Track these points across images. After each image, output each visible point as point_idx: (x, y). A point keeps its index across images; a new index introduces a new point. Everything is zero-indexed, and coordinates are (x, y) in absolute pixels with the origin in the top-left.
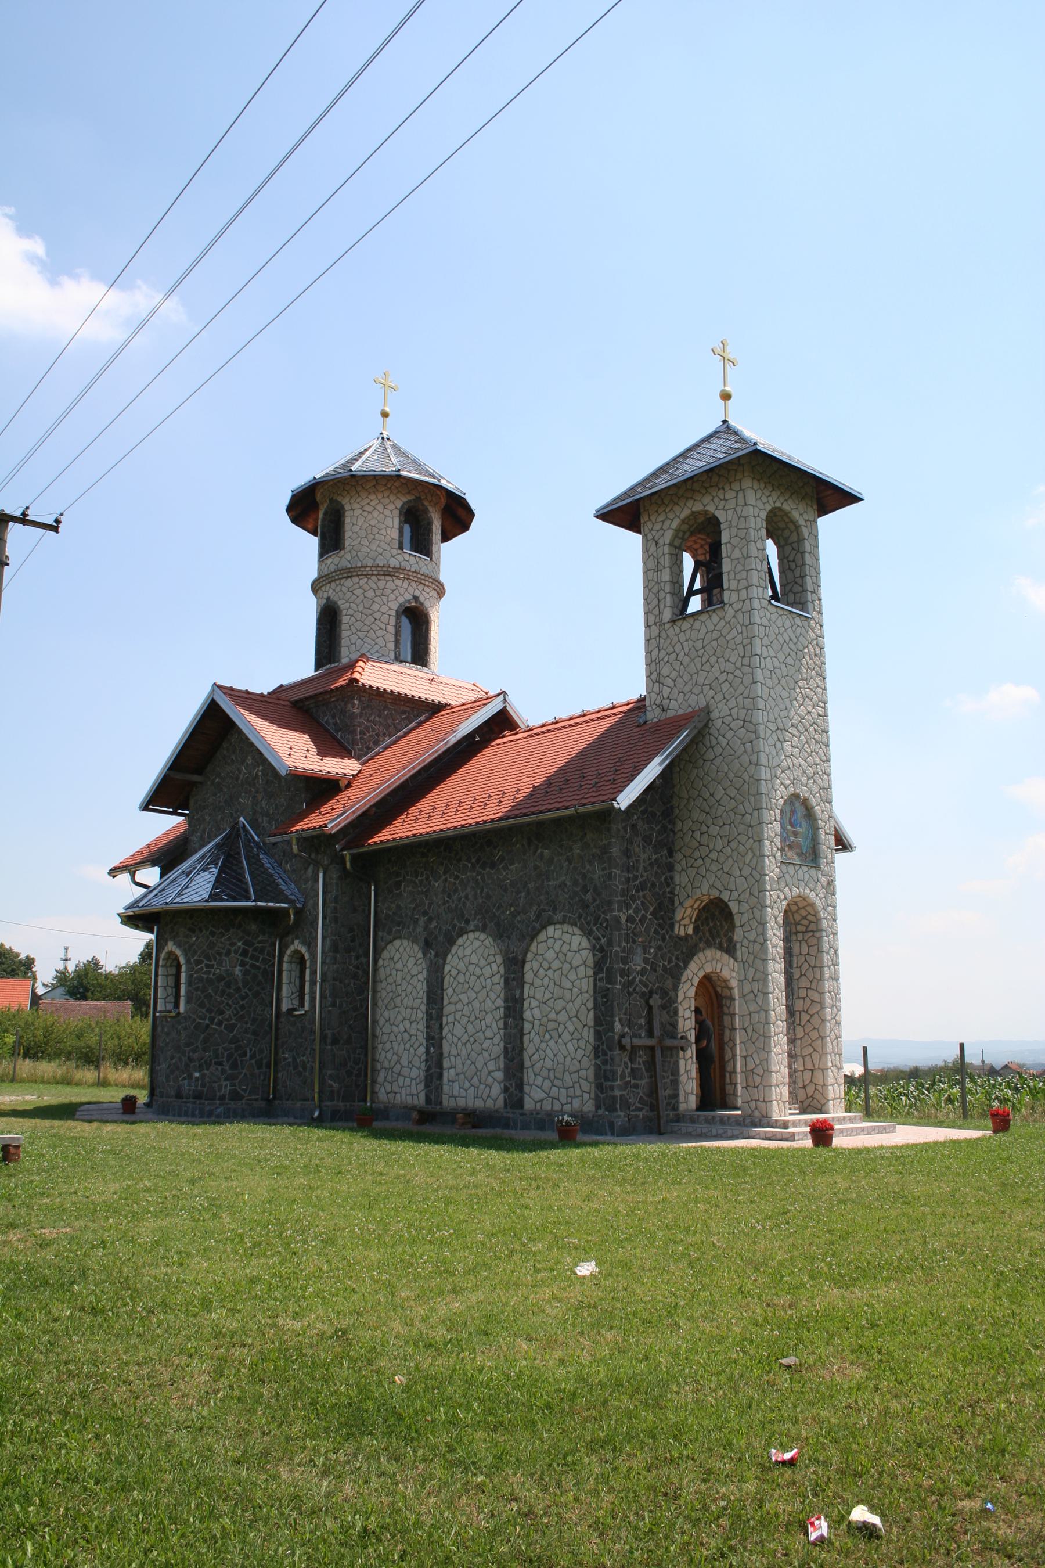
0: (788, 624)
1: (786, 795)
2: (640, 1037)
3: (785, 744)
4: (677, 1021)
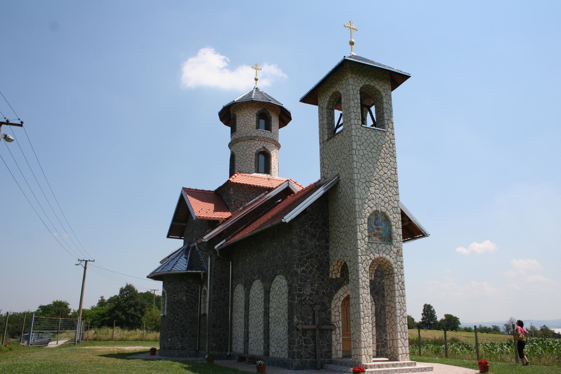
0: (373, 134)
1: (371, 211)
2: (309, 325)
3: (370, 188)
4: (331, 317)
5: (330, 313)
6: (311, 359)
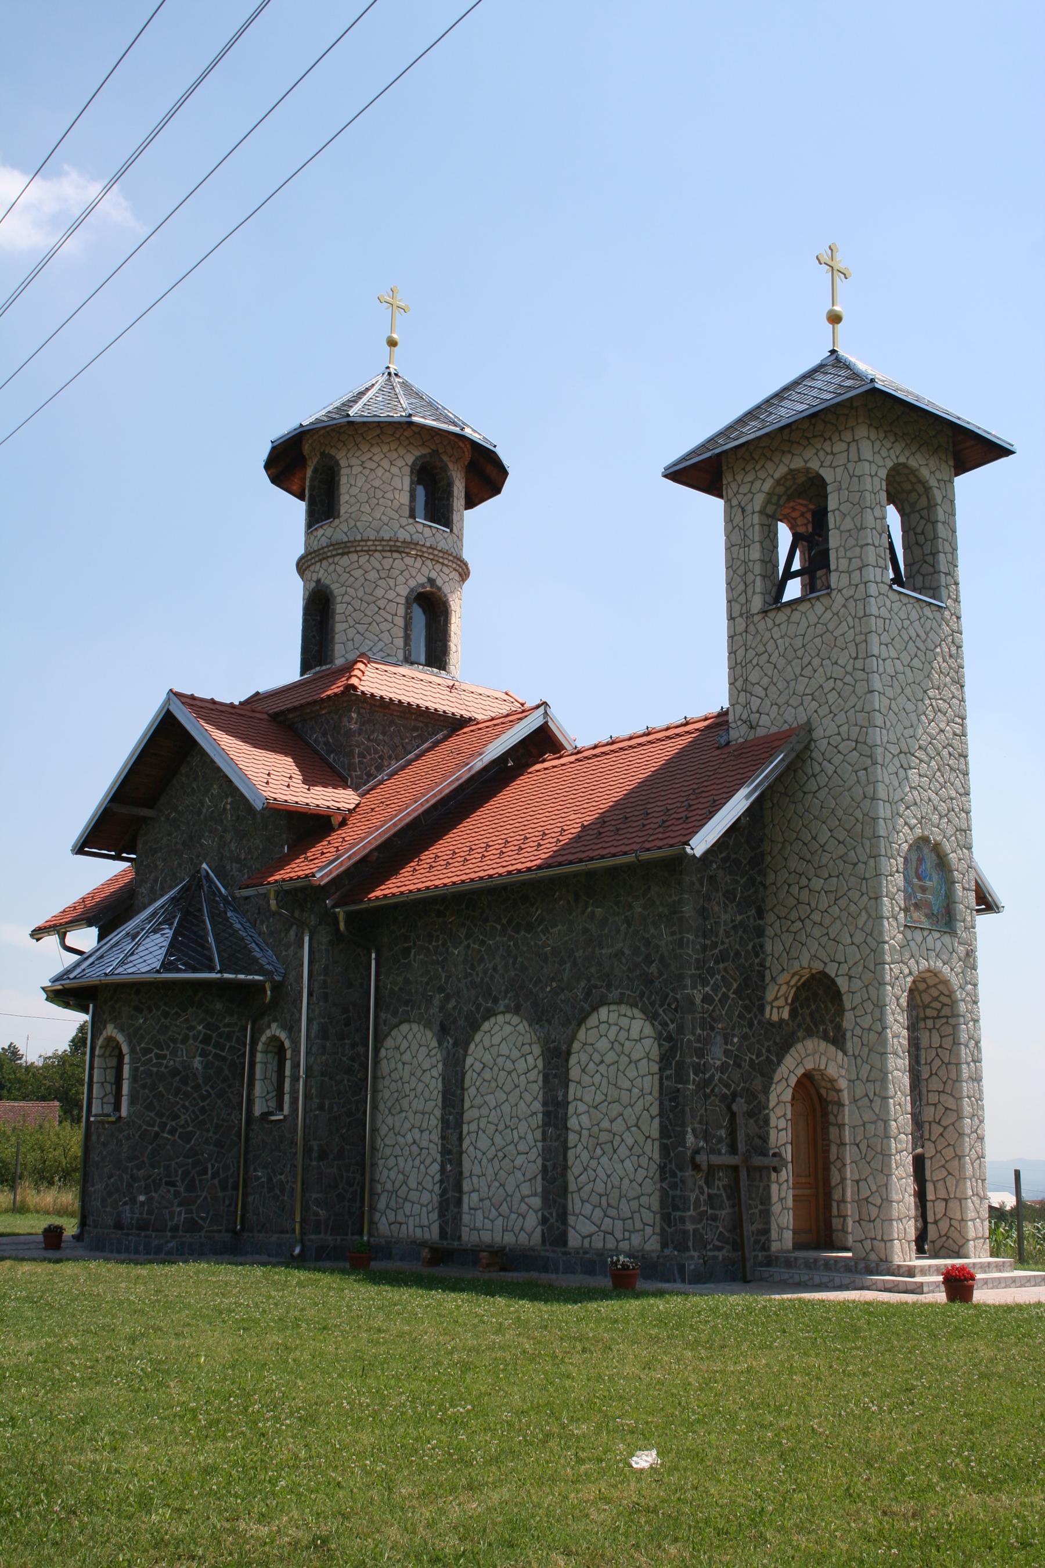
0: (914, 615)
2: (720, 1153)
3: (910, 772)
4: (768, 1133)
5: (767, 1121)
6: (724, 1252)
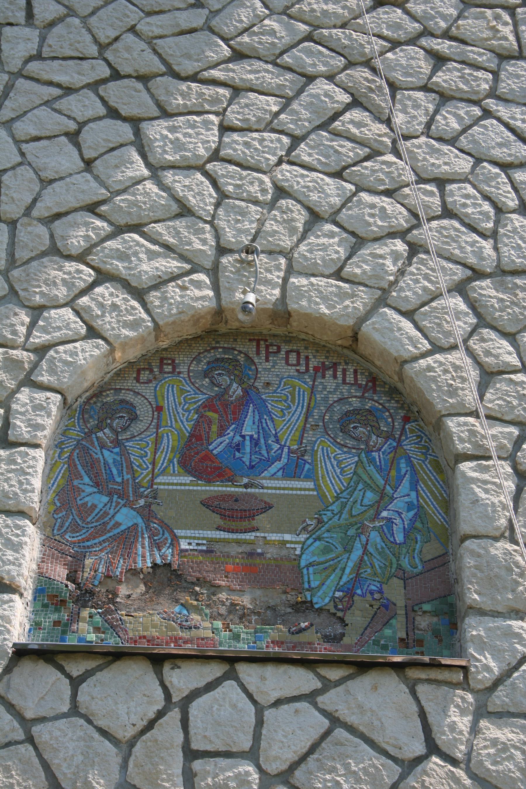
1: (124, 319)
